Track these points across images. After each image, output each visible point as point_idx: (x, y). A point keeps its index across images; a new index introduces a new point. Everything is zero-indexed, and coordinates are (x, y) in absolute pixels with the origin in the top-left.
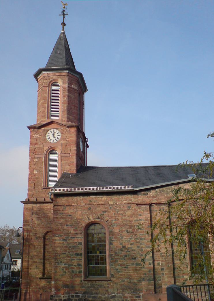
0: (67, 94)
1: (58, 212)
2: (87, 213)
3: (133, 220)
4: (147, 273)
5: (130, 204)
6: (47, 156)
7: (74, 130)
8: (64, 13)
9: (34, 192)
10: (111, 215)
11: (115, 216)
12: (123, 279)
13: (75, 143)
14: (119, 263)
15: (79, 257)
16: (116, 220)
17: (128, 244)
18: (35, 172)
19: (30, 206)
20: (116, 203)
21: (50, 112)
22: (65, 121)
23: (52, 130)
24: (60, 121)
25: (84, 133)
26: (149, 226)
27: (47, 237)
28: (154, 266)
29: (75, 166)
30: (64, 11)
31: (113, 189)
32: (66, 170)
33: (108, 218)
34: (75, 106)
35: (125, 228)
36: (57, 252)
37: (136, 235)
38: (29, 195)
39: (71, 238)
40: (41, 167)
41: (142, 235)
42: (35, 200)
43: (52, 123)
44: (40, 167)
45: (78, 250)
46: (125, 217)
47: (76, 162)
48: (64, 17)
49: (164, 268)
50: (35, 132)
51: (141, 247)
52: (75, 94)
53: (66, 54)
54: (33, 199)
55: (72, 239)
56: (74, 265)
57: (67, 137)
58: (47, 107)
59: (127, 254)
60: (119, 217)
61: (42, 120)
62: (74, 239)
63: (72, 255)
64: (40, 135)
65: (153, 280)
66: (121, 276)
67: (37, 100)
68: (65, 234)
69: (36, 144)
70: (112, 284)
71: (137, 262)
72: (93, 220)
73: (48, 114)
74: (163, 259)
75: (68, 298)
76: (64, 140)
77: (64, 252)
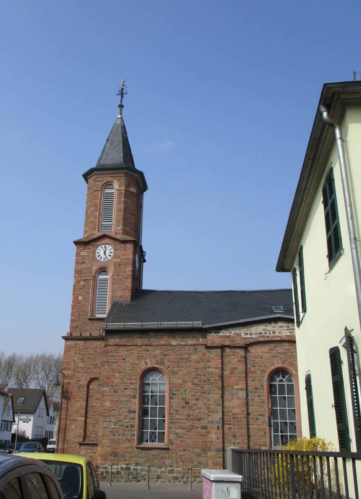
0: (123, 199)
1: (110, 354)
2: (145, 357)
3: (200, 368)
4: (214, 441)
5: (198, 346)
6: (95, 278)
7: (130, 247)
8: (122, 92)
9: (78, 324)
10: (173, 360)
11: (178, 362)
12: (184, 447)
13: (131, 262)
14: (181, 425)
15: (131, 415)
16: (179, 367)
17: (192, 400)
18: (80, 298)
19: (72, 343)
20: (180, 344)
21: (101, 223)
22: (119, 234)
23: (103, 246)
24: (113, 235)
25: (141, 246)
26: (219, 376)
27: (92, 385)
28: (223, 431)
29: (130, 291)
30: (122, 89)
31: (178, 325)
32: (118, 296)
33: (170, 364)
34: (132, 214)
35: (190, 377)
36: (107, 407)
37: (202, 387)
38: (71, 327)
39: (124, 389)
40: (88, 293)
41: (210, 388)
42: (79, 335)
43: (104, 236)
44: (86, 293)
45: (131, 406)
46: (190, 363)
47: (131, 287)
48: (122, 97)
49: (236, 435)
50: (82, 248)
51: (209, 405)
52: (133, 198)
53: (124, 148)
54: (76, 334)
55: (125, 390)
56: (125, 426)
57: (121, 255)
58: (98, 217)
59: (190, 414)
60: (183, 362)
61: (92, 232)
62: (127, 390)
63: (124, 412)
64: (87, 252)
65: (222, 450)
66: (182, 444)
67: (85, 206)
68: (117, 383)
69: (83, 263)
70: (170, 454)
71: (202, 424)
72: (151, 366)
73: (99, 225)
74: (235, 422)
75: (117, 470)
76: (117, 258)
77: (114, 408)
